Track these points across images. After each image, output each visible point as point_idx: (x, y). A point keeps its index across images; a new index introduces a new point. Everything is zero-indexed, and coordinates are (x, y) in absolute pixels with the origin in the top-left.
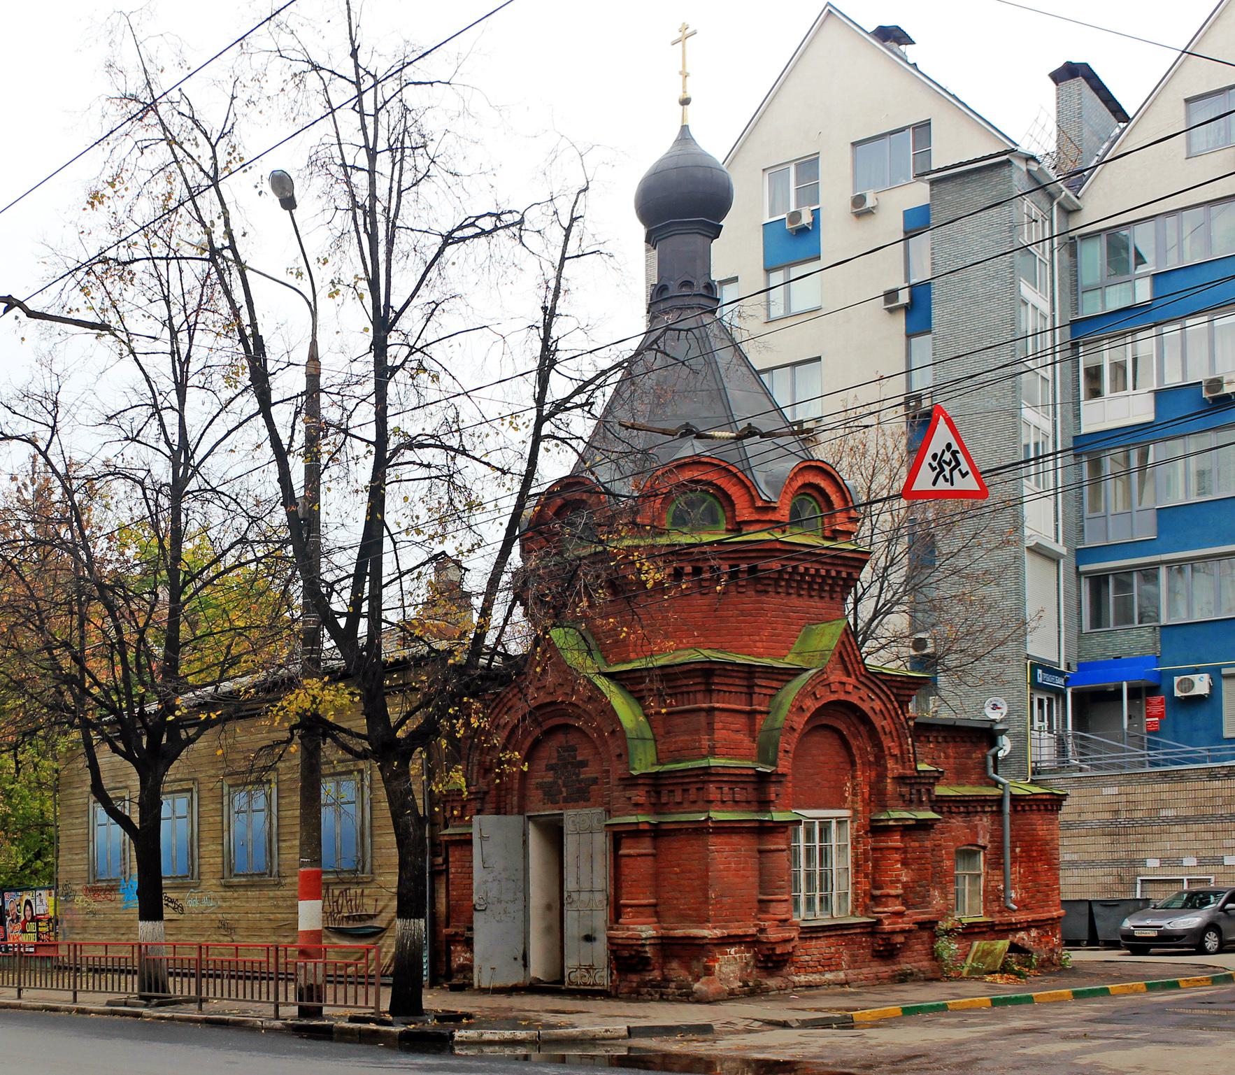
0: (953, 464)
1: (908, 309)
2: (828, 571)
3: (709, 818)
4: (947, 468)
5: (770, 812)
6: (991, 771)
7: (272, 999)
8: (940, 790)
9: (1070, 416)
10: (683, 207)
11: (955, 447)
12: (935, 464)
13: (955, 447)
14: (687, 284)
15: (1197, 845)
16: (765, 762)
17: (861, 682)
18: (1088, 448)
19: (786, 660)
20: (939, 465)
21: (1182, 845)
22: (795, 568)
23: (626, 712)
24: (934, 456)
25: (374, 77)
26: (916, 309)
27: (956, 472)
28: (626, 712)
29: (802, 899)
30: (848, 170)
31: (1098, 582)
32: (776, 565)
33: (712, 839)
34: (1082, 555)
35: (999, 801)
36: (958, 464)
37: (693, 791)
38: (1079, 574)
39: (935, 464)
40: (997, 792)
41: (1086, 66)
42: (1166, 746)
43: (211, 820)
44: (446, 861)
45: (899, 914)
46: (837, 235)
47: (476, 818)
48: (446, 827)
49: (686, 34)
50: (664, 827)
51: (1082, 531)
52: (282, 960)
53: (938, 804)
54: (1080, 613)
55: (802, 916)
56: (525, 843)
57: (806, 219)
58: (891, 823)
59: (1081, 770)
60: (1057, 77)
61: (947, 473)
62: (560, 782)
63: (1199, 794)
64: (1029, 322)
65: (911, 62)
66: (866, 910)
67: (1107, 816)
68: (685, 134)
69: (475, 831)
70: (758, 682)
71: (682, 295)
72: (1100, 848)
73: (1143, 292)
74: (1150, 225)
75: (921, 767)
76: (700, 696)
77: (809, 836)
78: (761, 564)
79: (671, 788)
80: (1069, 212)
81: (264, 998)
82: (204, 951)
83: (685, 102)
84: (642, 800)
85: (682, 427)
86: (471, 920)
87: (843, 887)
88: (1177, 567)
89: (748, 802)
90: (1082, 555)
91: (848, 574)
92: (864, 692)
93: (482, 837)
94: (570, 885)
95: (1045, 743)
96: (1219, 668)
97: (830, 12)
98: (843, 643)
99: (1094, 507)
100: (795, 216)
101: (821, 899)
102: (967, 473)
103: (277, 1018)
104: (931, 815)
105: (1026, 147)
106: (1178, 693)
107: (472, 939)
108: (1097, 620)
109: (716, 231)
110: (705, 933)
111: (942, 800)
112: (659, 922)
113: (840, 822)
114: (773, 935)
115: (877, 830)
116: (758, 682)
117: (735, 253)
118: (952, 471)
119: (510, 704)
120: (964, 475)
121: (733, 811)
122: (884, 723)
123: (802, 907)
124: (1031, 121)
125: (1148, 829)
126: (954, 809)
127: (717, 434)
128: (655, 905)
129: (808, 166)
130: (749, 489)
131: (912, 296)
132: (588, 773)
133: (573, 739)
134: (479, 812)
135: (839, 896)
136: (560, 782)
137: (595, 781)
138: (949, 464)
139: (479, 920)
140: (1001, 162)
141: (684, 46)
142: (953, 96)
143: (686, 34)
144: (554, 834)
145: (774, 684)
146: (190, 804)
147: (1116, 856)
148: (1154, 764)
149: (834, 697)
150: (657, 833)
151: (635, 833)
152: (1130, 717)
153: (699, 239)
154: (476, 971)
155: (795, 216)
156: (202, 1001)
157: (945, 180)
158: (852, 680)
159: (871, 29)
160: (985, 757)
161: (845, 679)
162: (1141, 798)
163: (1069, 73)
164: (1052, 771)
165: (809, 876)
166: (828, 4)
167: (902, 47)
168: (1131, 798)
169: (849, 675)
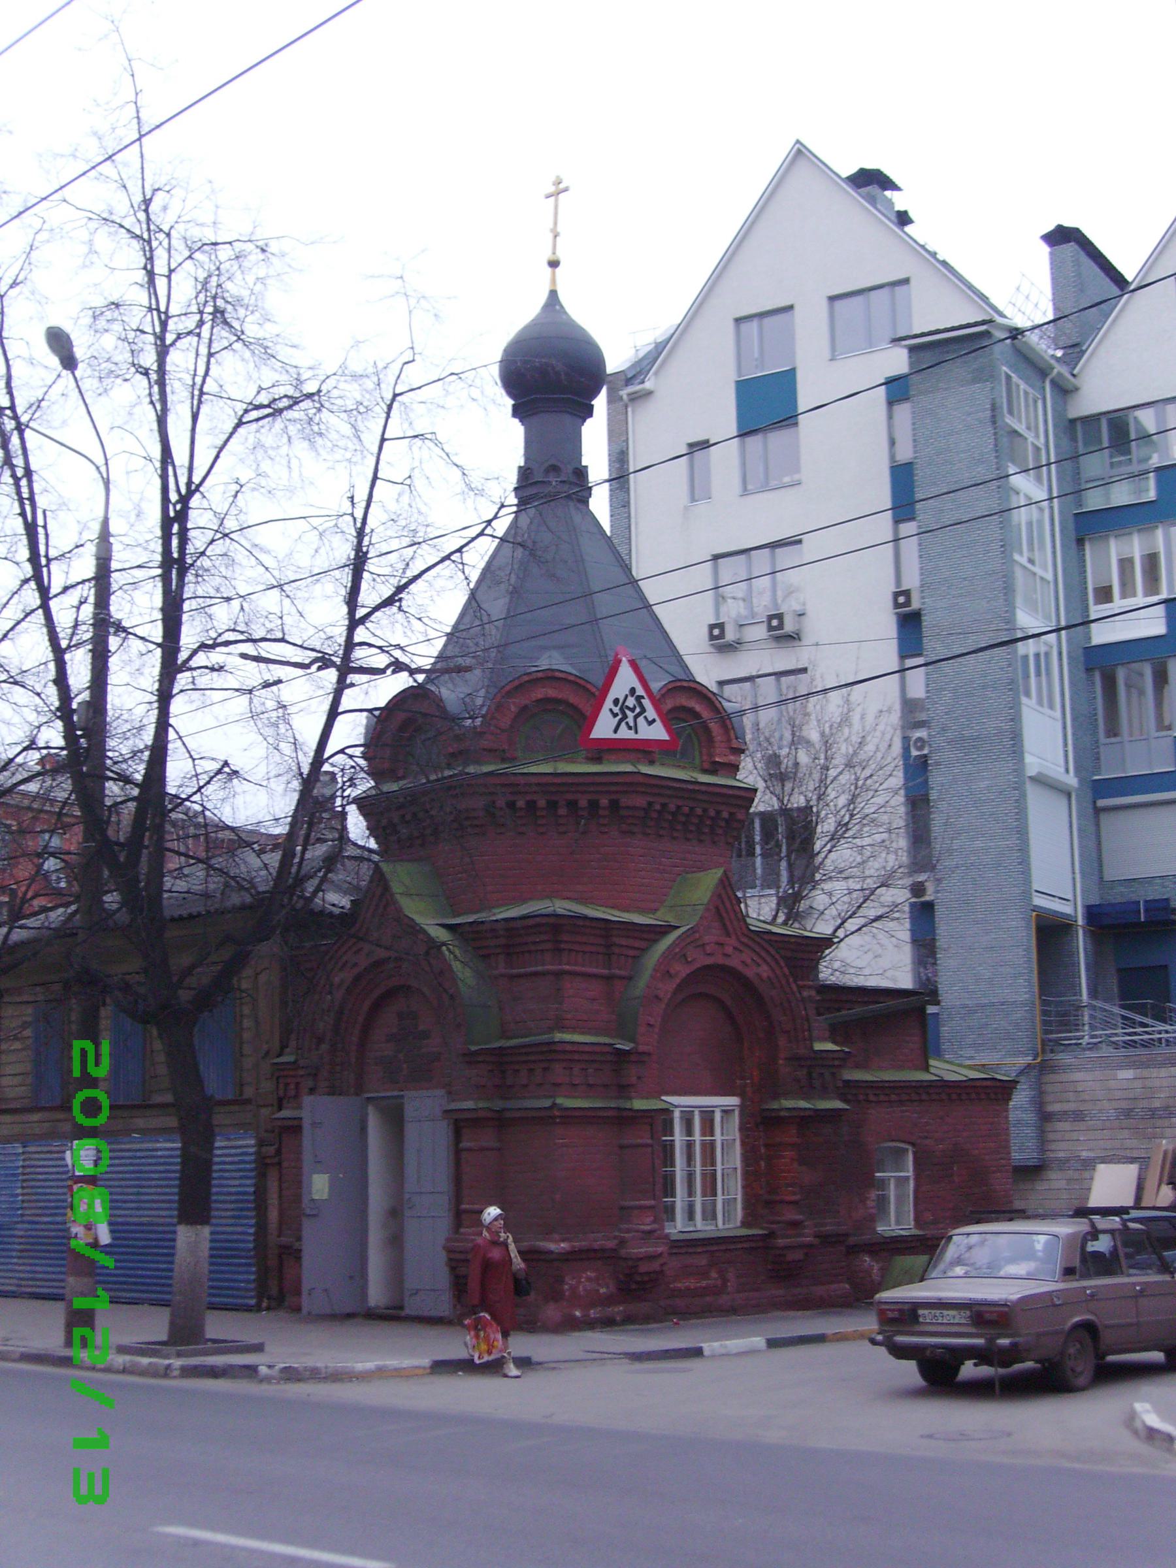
0: (638, 710)
2: (705, 810)
3: (554, 1104)
4: (630, 715)
5: (630, 1098)
10: (551, 379)
11: (640, 691)
12: (616, 710)
14: (554, 469)
16: (624, 1037)
17: (742, 943)
18: (1102, 667)
19: (659, 914)
22: (664, 805)
23: (463, 972)
24: (616, 702)
27: (641, 720)
28: (463, 972)
32: (640, 801)
36: (643, 710)
39: (616, 710)
41: (1077, 230)
45: (795, 1224)
49: (559, 190)
50: (508, 1115)
51: (1098, 759)
55: (678, 1227)
56: (363, 1130)
58: (782, 1114)
62: (401, 1056)
70: (616, 940)
71: (549, 482)
75: (819, 1046)
78: (625, 801)
79: (517, 1067)
80: (1065, 391)
83: (554, 264)
86: (299, 1229)
89: (606, 1086)
91: (731, 814)
92: (746, 956)
94: (410, 1186)
97: (800, 153)
98: (720, 896)
102: (654, 721)
104: (838, 1104)
110: (552, 1246)
113: (726, 1112)
114: (638, 1250)
116: (566, 937)
118: (636, 717)
119: (345, 958)
120: (651, 723)
126: (872, 1098)
134: (312, 1091)
138: (632, 710)
141: (556, 201)
143: (559, 190)
144: (395, 1120)
145: (638, 944)
149: (709, 961)
153: (567, 419)
158: (733, 941)
162: (1157, 1083)
165: (690, 1177)
166: (798, 142)
167: (888, 193)
169: (728, 935)
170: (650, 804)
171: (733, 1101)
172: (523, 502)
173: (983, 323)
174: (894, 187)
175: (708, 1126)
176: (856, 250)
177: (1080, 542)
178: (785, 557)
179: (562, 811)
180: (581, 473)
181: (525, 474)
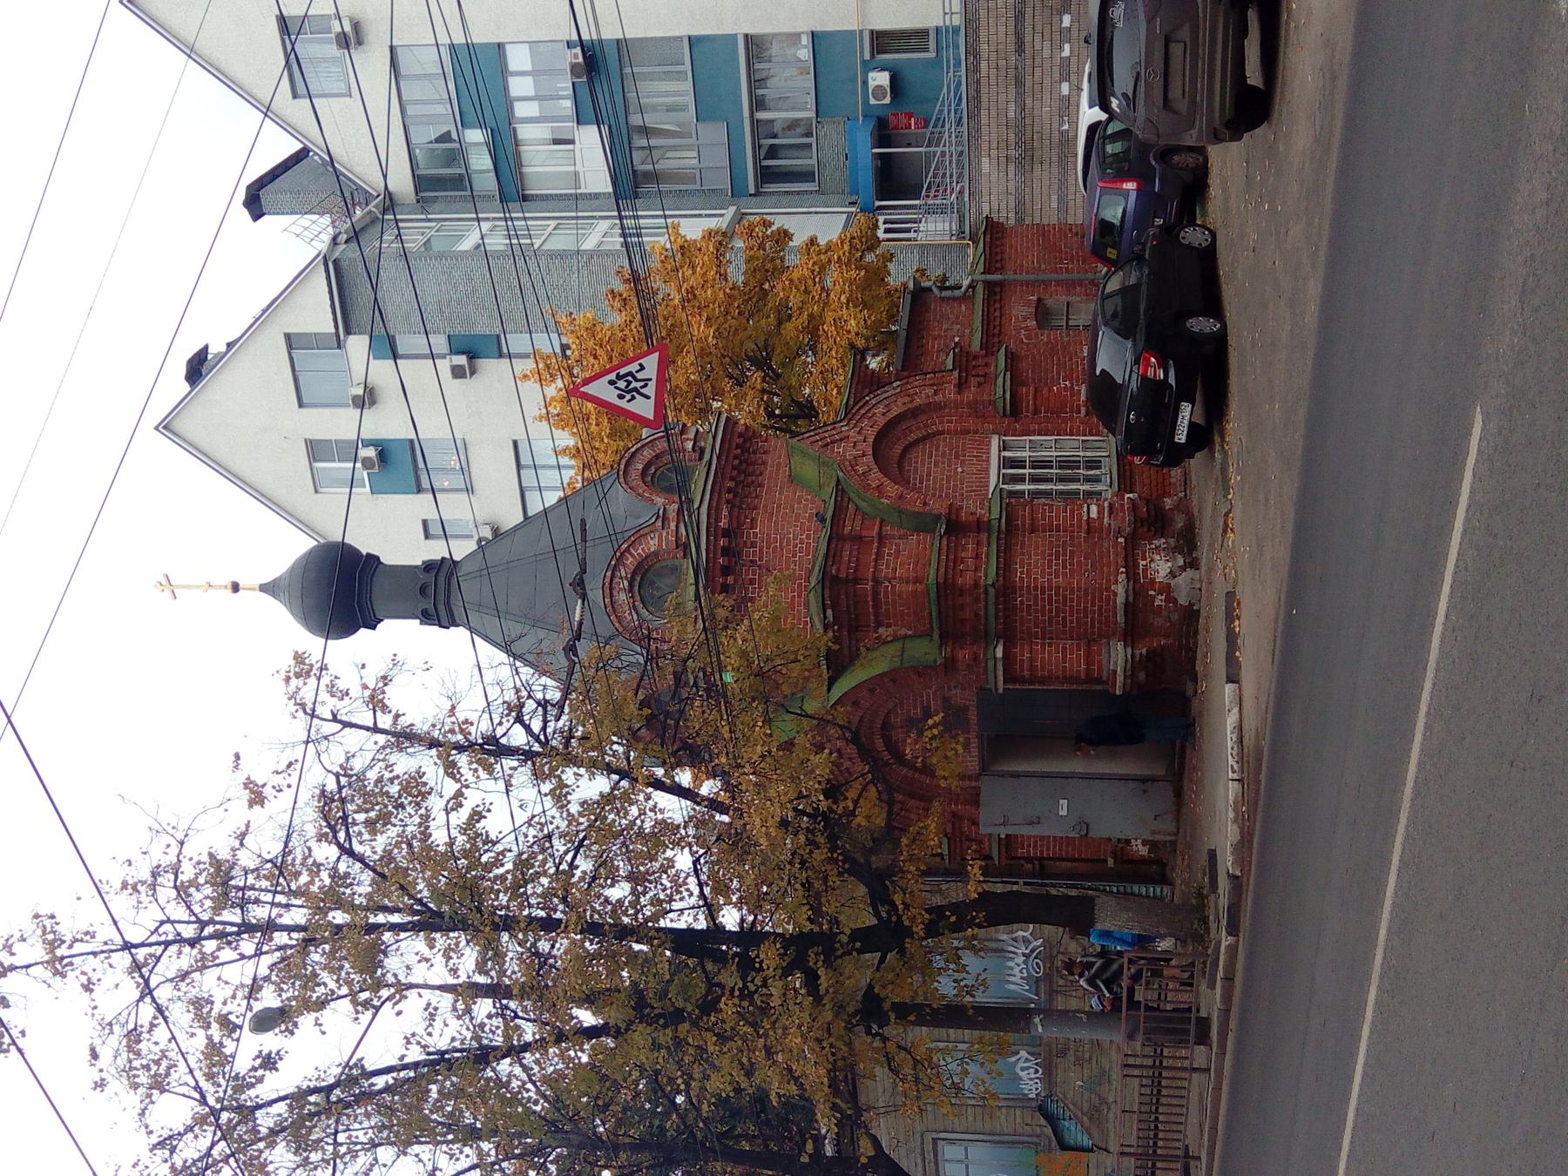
1: (472, 356)
4: (634, 384)
6: (957, 293)
7: (1186, 1075)
8: (976, 346)
9: (597, 202)
10: (342, 590)
11: (613, 376)
12: (628, 397)
13: (613, 376)
15: (1047, 81)
18: (631, 184)
20: (631, 392)
21: (1046, 96)
24: (621, 397)
25: (162, 923)
26: (471, 351)
27: (639, 376)
29: (1086, 487)
30: (327, 412)
31: (767, 176)
33: (1019, 572)
34: (737, 192)
35: (987, 284)
36: (630, 374)
38: (757, 194)
39: (628, 397)
40: (980, 288)
42: (941, 111)
43: (971, 1119)
44: (1029, 860)
46: (387, 423)
47: (983, 830)
49: (167, 584)
52: (1138, 1061)
53: (989, 347)
54: (798, 193)
57: (371, 452)
59: (961, 192)
60: (257, 214)
61: (638, 385)
63: (993, 82)
64: (497, 242)
65: (224, 349)
67: (1012, 168)
68: (268, 588)
69: (1003, 832)
71: (435, 594)
72: (1046, 174)
73: (475, 136)
74: (412, 129)
77: (1020, 479)
81: (1186, 1084)
82: (1126, 1150)
83: (236, 588)
85: (567, 656)
87: (1076, 444)
88: (758, 104)
90: (737, 192)
93: (1004, 824)
95: (931, 227)
96: (864, 62)
97: (166, 427)
99: (691, 179)
100: (367, 463)
101: (1088, 468)
103: (1208, 1070)
105: (322, 244)
106: (887, 100)
107: (1220, 342)
108: (806, 176)
109: (373, 560)
111: (985, 345)
113: (1005, 447)
115: (1015, 411)
117: (393, 533)
118: (637, 380)
120: (642, 368)
123: (1099, 487)
124: (295, 240)
125: (1028, 129)
127: (577, 618)
129: (316, 450)
130: (640, 534)
131: (457, 353)
134: (975, 823)
135: (1085, 449)
138: (629, 383)
139: (1100, 831)
140: (336, 270)
142: (264, 311)
143: (167, 584)
146: (952, 1142)
147: (1055, 159)
148: (959, 123)
152: (909, 145)
154: (1157, 837)
155: (367, 463)
156: (1187, 1156)
157: (347, 320)
159: (186, 387)
160: (943, 299)
163: (255, 203)
164: (961, 221)
165: (1061, 480)
166: (156, 428)
168: (994, 146)
170: (728, 502)
171: (995, 442)
172: (451, 622)
173: (326, 264)
174: (206, 347)
175: (1018, 463)
176: (257, 390)
177: (525, 198)
178: (525, 459)
179: (730, 580)
180: (429, 566)
181: (428, 618)
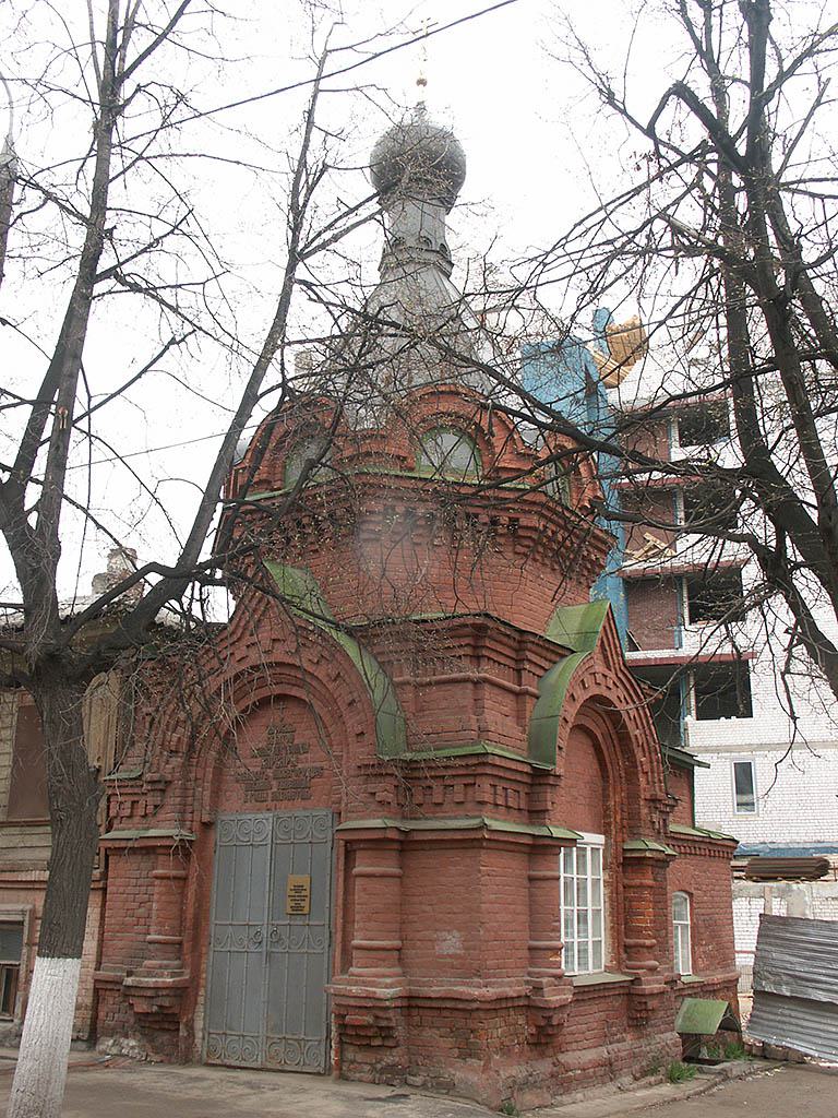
37: (459, 788)
48: (108, 831)
58: (648, 854)
66: (618, 969)
76: (465, 662)
84: (390, 797)
112: (404, 974)
121: (505, 820)
122: (637, 732)
128: (399, 950)
132: (307, 762)
133: (291, 714)
136: (270, 773)
137: (319, 772)
150: (406, 845)
151: (377, 843)
158: (611, 675)
161: (607, 672)
